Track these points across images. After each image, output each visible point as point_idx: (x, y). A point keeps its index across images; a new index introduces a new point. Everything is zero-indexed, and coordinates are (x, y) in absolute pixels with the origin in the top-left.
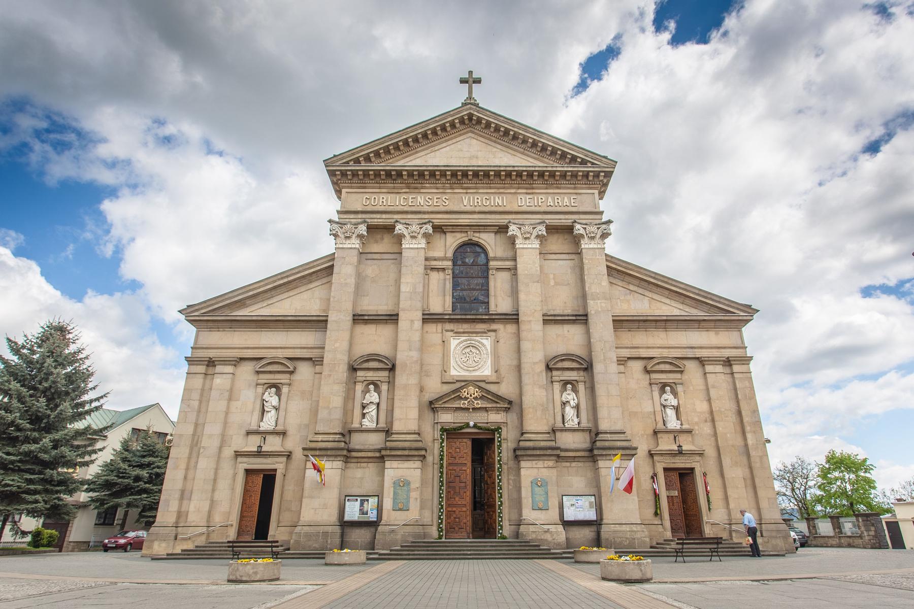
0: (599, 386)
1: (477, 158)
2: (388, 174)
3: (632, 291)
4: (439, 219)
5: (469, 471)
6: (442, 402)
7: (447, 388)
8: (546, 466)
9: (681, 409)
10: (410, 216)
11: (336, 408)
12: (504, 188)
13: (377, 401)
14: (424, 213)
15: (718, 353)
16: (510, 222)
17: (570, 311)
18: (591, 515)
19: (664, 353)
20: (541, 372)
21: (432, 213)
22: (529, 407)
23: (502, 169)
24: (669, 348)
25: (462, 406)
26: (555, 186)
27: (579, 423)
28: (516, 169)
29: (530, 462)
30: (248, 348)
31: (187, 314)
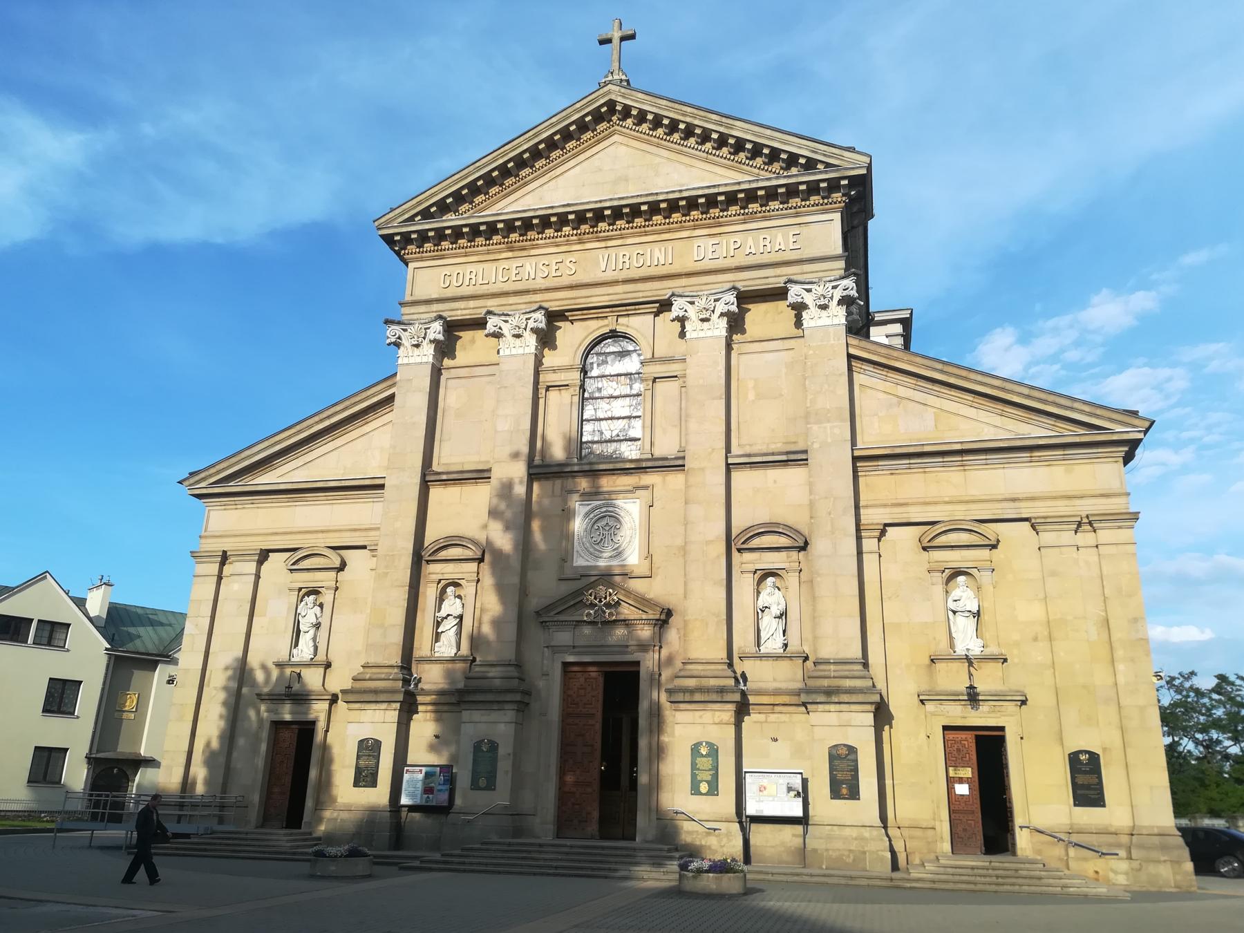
0: (819, 579)
1: (627, 180)
2: (475, 231)
3: (902, 398)
4: (556, 302)
5: (598, 727)
6: (555, 612)
7: (566, 588)
8: (717, 720)
9: (986, 618)
10: (512, 300)
11: (394, 626)
12: (669, 231)
13: (458, 611)
14: (535, 291)
15: (1067, 509)
16: (673, 295)
17: (779, 445)
18: (798, 811)
19: (956, 513)
20: (718, 557)
21: (547, 290)
22: (696, 619)
23: (661, 197)
24: (967, 502)
25: (585, 619)
26: (759, 215)
27: (786, 645)
28: (685, 194)
29: (691, 713)
30: (276, 534)
31: (190, 485)
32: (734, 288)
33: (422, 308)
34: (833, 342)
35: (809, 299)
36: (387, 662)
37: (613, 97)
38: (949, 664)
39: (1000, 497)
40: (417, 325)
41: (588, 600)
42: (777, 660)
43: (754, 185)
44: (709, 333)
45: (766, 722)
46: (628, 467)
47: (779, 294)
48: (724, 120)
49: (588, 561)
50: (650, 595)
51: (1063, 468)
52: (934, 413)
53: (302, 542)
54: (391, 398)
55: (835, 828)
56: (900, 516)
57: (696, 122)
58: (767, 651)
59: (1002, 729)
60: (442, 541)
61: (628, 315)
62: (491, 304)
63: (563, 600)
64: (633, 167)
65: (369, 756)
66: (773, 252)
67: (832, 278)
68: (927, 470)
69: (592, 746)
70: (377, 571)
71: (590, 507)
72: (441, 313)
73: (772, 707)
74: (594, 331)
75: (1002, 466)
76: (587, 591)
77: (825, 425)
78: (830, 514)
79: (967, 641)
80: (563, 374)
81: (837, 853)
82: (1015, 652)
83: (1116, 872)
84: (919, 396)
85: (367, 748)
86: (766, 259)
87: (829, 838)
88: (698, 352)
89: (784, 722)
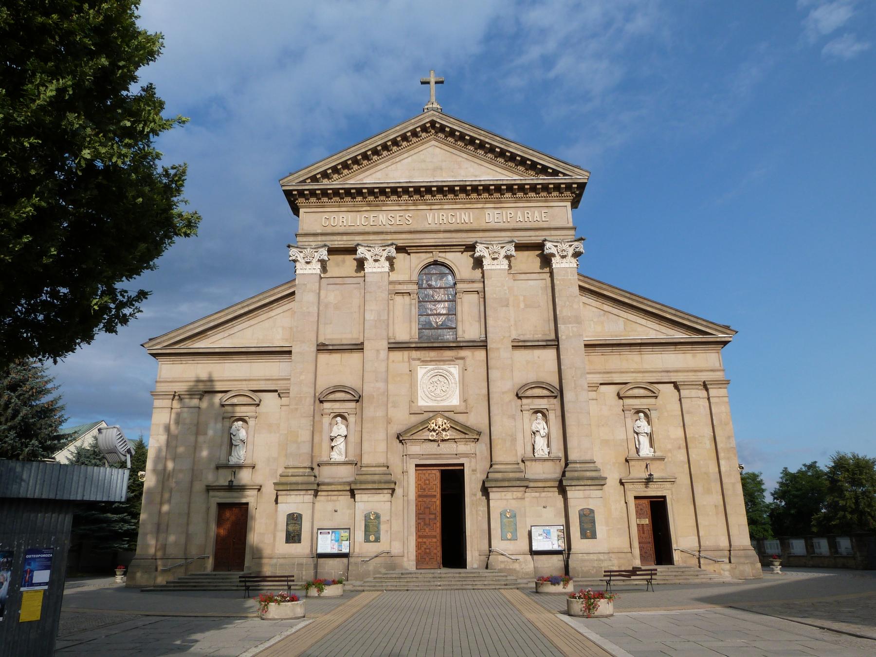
1: (441, 169)
8: (515, 497)
10: (372, 237)
11: (304, 442)
14: (387, 233)
15: (694, 377)
17: (540, 336)
21: (395, 233)
23: (468, 183)
28: (483, 183)
31: (148, 347)
32: (325, 246)
33: (311, 239)
34: (570, 277)
35: (368, 255)
36: (301, 465)
37: (435, 119)
38: (640, 462)
39: (660, 370)
40: (308, 250)
41: (431, 427)
42: (544, 461)
43: (524, 182)
44: (498, 267)
45: (540, 497)
46: (451, 345)
47: (352, 251)
48: (504, 141)
49: (427, 402)
50: (468, 424)
51: (691, 354)
52: (624, 321)
53: (230, 386)
54: (293, 293)
55: (584, 555)
56: (607, 379)
57: (487, 140)
58: (539, 456)
59: (664, 497)
60: (331, 388)
61: (445, 252)
62: (358, 239)
63: (415, 426)
64: (445, 161)
65: (295, 524)
66: (347, 226)
67: (570, 240)
68: (621, 353)
69: (435, 514)
70: (290, 407)
71: (427, 369)
72: (325, 243)
73: (543, 488)
74: (424, 260)
75: (660, 352)
76: (430, 421)
77: (568, 325)
78: (573, 377)
79: (646, 451)
80: (405, 285)
81: (587, 569)
82: (670, 455)
83: (724, 570)
84: (615, 311)
85: (293, 519)
86: (528, 225)
87: (583, 561)
88: (492, 278)
89: (550, 497)
